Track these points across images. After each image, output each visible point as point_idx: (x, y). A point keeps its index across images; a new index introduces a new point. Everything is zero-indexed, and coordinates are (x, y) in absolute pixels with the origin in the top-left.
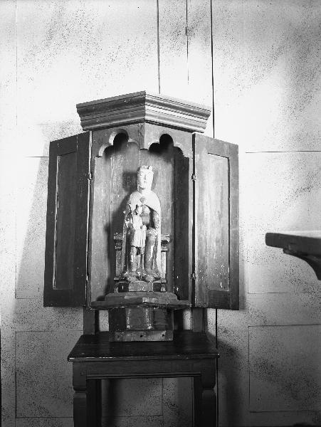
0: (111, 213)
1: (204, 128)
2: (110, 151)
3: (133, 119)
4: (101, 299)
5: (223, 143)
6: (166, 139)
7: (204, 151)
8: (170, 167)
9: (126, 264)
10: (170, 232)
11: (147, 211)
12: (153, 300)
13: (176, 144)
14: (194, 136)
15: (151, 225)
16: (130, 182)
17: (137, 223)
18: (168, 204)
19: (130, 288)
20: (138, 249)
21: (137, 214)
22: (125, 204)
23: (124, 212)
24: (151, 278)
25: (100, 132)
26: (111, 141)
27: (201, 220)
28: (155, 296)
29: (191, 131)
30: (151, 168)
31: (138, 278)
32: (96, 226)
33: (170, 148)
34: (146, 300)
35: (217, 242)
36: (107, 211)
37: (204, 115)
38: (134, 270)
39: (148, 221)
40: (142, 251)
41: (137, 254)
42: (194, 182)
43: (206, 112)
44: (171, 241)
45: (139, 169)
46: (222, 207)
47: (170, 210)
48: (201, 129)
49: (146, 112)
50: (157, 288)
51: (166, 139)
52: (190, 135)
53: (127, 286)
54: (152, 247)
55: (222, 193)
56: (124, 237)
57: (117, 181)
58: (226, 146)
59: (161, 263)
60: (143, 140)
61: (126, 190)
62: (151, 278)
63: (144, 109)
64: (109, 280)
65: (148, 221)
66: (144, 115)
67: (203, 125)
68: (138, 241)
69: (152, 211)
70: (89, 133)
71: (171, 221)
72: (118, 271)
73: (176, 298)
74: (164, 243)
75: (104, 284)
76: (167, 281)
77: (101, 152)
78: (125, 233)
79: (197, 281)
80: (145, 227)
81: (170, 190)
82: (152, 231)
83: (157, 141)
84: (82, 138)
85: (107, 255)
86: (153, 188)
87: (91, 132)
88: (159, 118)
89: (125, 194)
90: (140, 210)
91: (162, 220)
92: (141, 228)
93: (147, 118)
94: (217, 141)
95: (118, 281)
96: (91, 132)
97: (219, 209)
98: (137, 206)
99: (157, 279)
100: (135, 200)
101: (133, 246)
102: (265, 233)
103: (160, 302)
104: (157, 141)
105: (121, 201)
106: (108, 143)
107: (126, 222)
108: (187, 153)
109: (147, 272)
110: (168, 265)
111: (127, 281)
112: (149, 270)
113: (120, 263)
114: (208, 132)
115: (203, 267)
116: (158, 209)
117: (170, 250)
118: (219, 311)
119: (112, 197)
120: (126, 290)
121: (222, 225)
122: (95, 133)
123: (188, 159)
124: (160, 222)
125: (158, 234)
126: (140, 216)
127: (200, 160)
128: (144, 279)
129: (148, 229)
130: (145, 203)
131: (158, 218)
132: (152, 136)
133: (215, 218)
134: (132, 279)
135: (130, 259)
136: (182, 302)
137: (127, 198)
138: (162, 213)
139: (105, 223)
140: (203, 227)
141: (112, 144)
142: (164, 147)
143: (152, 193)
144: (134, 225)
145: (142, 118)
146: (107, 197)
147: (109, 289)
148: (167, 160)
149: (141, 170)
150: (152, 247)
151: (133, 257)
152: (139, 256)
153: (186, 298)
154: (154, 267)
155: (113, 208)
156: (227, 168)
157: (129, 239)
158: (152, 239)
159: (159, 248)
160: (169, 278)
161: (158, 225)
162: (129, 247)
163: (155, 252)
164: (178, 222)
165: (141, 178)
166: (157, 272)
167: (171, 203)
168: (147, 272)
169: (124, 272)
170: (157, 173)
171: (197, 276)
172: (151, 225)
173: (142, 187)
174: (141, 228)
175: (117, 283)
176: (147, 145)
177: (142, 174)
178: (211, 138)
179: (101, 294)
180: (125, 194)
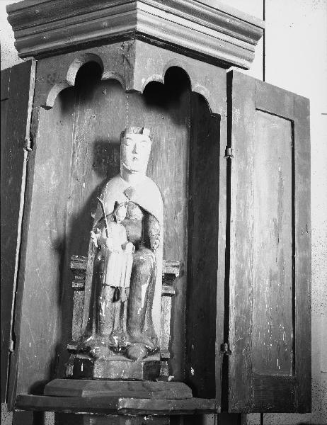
0: (68, 218)
1: (250, 60)
2: (72, 98)
3: (112, 31)
4: (38, 389)
5: (283, 93)
6: (177, 78)
7: (249, 106)
8: (181, 134)
9: (91, 316)
10: (179, 257)
11: (138, 215)
12: (143, 403)
13: (197, 87)
14: (230, 76)
15: (144, 242)
16: (108, 159)
17: (115, 239)
18: (178, 204)
19: (98, 372)
20: (117, 291)
21: (115, 221)
22: (93, 202)
23: (93, 216)
24: (139, 352)
25: (52, 60)
26: (71, 77)
27: (242, 234)
28: (146, 392)
29: (224, 64)
30: (147, 131)
31: (112, 348)
32: (36, 243)
33: (185, 99)
34: (125, 403)
35: (272, 278)
36: (60, 213)
37: (252, 34)
38: (107, 331)
39: (139, 235)
40: (124, 297)
41: (114, 300)
42: (229, 161)
43: (254, 30)
44: (182, 273)
45: (123, 134)
46: (280, 214)
47: (180, 215)
48: (246, 64)
49: (139, 16)
50: (152, 372)
51: (177, 78)
52: (223, 72)
53: (90, 366)
54: (144, 287)
55: (281, 185)
56: (90, 266)
57: (82, 158)
58: (288, 99)
59: (161, 317)
60: (133, 72)
61: (100, 173)
62: (139, 352)
63: (135, 8)
64: (59, 348)
65: (137, 233)
66: (135, 20)
67: (247, 54)
68: (117, 274)
69: (146, 214)
70: (29, 63)
71: (181, 238)
72: (77, 328)
73: (189, 393)
74: (168, 278)
75: (48, 356)
76: (172, 356)
77: (52, 98)
78: (91, 256)
79: (232, 359)
80: (130, 247)
81: (182, 178)
82: (145, 255)
83: (160, 77)
84: (20, 72)
85: (55, 297)
86: (150, 171)
87: (34, 63)
88: (165, 30)
89: (95, 181)
90: (122, 212)
91: (167, 233)
92: (123, 247)
93: (141, 27)
94: (273, 89)
95: (74, 352)
96: (34, 63)
97: (276, 216)
98: (116, 205)
99: (150, 352)
100: (114, 192)
101: (106, 285)
102: (66, 127)
103: (156, 407)
104: (160, 77)
105: (89, 194)
106: (66, 81)
107: (93, 235)
108: (218, 107)
109: (132, 338)
110: (176, 321)
111: (91, 355)
112: (136, 333)
113: (80, 316)
114: (255, 71)
115: (244, 326)
116: (157, 210)
117: (180, 293)
118: (266, 416)
119: (72, 184)
120: (88, 374)
121: (280, 247)
122: (43, 64)
123: (218, 117)
124: (161, 238)
125: (158, 261)
126: (122, 223)
127: (242, 119)
128: (125, 352)
129: (137, 249)
130: (134, 199)
131: (157, 229)
132: (148, 68)
133: (268, 234)
134: (100, 351)
135: (98, 308)
136: (201, 403)
137: (98, 192)
138: (165, 221)
139: (55, 236)
140: (246, 247)
141: (73, 83)
142: (170, 94)
143: (149, 178)
144: (110, 243)
145: (132, 27)
146: (60, 186)
147: (55, 368)
148: (178, 121)
149: (128, 135)
150: (144, 287)
151: (106, 305)
152: (118, 304)
153: (210, 394)
154: (146, 327)
155: (72, 206)
156: (291, 140)
157: (99, 269)
158: (144, 270)
159: (159, 288)
160: (175, 348)
161: (159, 241)
162: (98, 286)
163: (150, 297)
164: (196, 238)
165: (128, 150)
166: (153, 337)
167: (182, 200)
168: (132, 338)
169: (87, 336)
170: (159, 144)
171: (233, 348)
172: (144, 242)
173: (128, 168)
174: (123, 247)
175: (70, 360)
176: (140, 83)
177: (128, 142)
178: (260, 81)
179: (40, 376)
180: (95, 181)
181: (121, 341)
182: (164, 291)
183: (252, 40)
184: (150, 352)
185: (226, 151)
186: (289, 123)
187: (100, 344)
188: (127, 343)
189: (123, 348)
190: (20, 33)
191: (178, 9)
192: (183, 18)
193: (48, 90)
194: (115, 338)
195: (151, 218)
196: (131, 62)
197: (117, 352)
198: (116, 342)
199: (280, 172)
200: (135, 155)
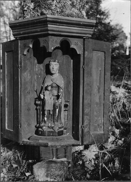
31: (48, 127)
45: (49, 62)
54: (57, 110)
181: (51, 125)
182: (64, 109)
183: (91, 28)
184: (60, 128)
185: (83, 66)
186: (103, 53)
187: (45, 126)
188: (53, 126)
189: (52, 127)
190: (14, 31)
191: (54, 32)
192: (104, 86)
193: (24, 50)
194: (50, 124)
195: (60, 88)
196: (48, 43)
197: (50, 128)
198: (50, 125)
199: (100, 71)
200: (53, 69)
